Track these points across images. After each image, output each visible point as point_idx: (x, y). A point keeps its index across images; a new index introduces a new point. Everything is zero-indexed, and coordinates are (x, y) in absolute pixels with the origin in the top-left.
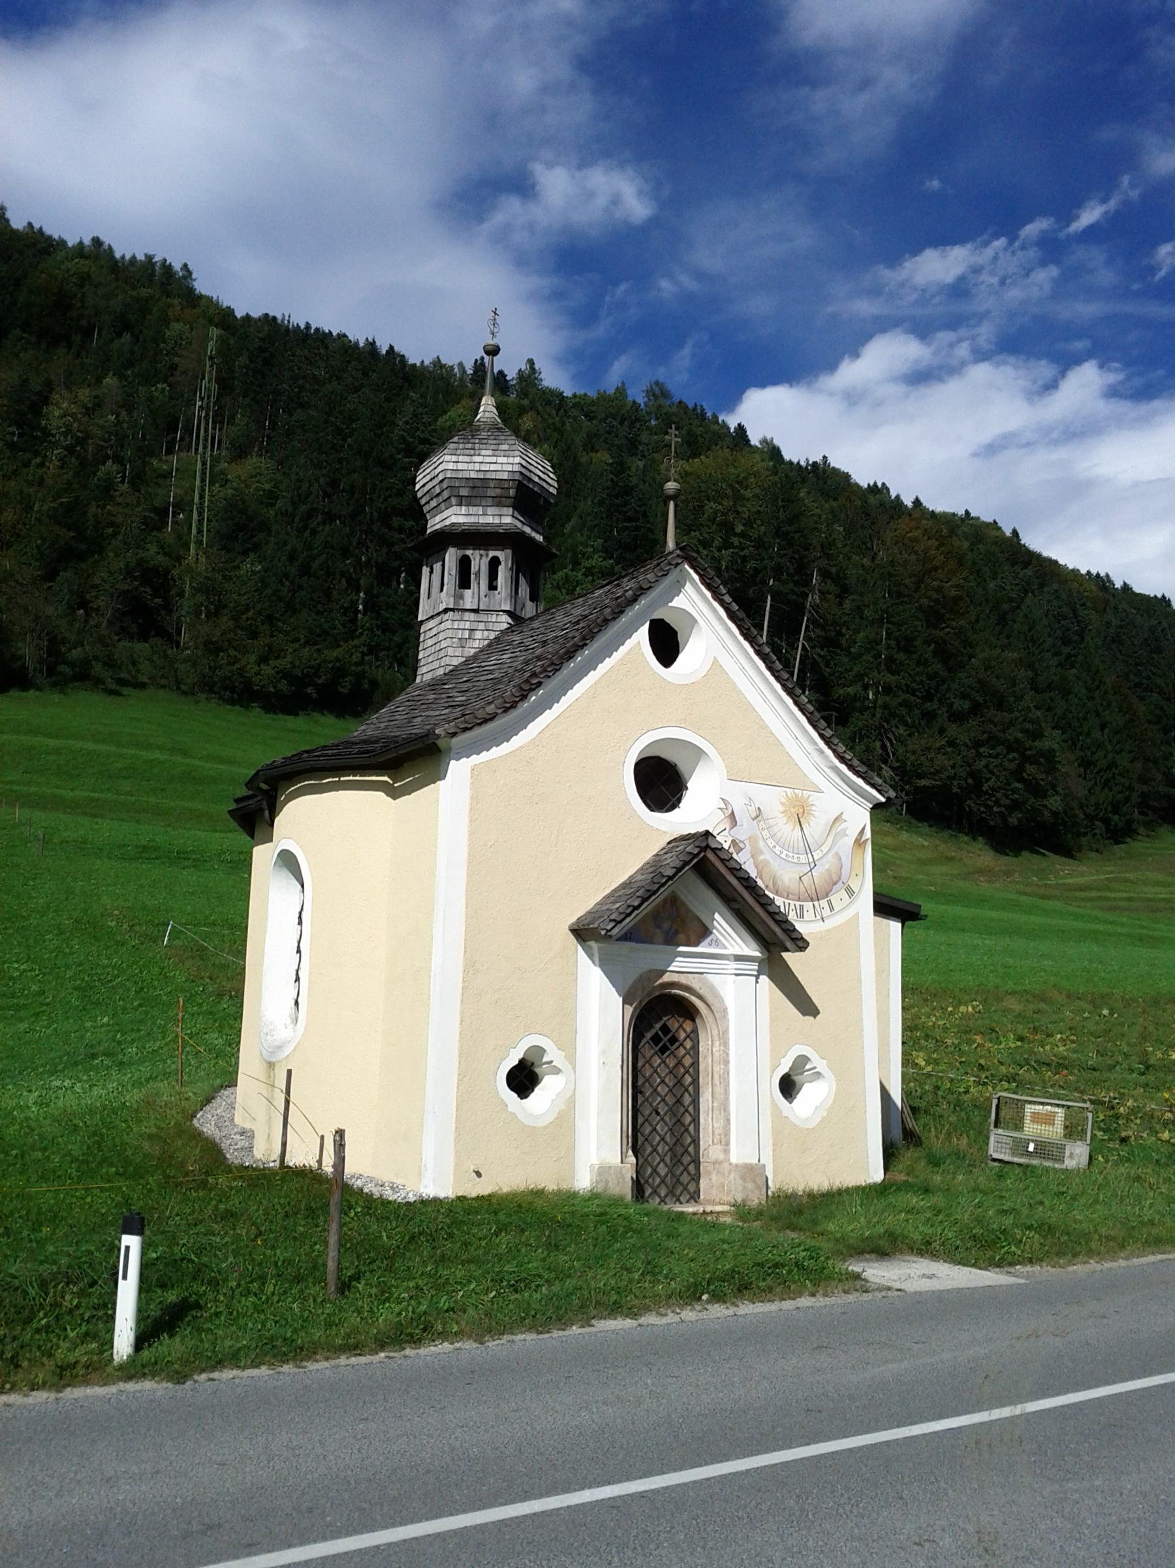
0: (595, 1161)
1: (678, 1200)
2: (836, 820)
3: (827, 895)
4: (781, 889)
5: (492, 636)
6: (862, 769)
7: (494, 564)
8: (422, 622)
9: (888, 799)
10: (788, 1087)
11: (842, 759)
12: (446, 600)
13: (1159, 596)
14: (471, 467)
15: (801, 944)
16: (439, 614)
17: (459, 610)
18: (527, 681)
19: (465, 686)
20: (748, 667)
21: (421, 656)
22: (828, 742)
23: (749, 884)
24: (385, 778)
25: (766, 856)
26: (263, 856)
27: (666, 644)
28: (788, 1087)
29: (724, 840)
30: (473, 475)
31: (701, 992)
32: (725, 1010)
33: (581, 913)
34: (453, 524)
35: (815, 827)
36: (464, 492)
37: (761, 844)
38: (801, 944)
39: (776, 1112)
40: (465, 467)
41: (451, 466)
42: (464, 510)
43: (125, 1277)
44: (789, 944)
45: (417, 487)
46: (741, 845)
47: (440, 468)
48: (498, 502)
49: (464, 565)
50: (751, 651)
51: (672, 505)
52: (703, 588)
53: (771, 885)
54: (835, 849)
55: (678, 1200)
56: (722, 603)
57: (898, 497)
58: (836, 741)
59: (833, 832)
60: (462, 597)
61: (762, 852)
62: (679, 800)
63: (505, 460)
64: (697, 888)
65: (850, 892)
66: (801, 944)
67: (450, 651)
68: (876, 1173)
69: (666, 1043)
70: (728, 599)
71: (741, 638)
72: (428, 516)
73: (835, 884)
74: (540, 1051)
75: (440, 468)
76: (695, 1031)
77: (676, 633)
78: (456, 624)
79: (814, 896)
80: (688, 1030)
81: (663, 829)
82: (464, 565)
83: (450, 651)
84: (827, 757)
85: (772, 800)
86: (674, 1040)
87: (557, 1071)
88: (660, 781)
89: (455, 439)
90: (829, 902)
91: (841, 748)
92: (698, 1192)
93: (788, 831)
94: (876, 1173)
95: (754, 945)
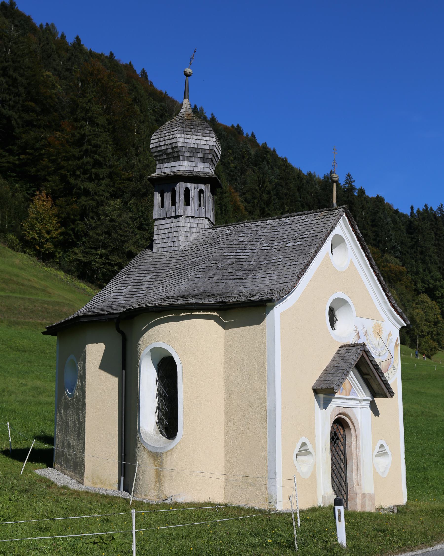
0: (323, 493)
6: (400, 311)
8: (155, 219)
9: (407, 325)
14: (191, 141)
30: (192, 146)
36: (187, 154)
38: (392, 394)
40: (188, 141)
41: (181, 140)
43: (340, 520)
48: (204, 159)
49: (187, 191)
60: (187, 210)
63: (208, 139)
65: (394, 368)
68: (400, 497)
71: (361, 249)
73: (390, 365)
82: (187, 191)
84: (387, 305)
85: (369, 325)
94: (400, 497)
95: (369, 394)
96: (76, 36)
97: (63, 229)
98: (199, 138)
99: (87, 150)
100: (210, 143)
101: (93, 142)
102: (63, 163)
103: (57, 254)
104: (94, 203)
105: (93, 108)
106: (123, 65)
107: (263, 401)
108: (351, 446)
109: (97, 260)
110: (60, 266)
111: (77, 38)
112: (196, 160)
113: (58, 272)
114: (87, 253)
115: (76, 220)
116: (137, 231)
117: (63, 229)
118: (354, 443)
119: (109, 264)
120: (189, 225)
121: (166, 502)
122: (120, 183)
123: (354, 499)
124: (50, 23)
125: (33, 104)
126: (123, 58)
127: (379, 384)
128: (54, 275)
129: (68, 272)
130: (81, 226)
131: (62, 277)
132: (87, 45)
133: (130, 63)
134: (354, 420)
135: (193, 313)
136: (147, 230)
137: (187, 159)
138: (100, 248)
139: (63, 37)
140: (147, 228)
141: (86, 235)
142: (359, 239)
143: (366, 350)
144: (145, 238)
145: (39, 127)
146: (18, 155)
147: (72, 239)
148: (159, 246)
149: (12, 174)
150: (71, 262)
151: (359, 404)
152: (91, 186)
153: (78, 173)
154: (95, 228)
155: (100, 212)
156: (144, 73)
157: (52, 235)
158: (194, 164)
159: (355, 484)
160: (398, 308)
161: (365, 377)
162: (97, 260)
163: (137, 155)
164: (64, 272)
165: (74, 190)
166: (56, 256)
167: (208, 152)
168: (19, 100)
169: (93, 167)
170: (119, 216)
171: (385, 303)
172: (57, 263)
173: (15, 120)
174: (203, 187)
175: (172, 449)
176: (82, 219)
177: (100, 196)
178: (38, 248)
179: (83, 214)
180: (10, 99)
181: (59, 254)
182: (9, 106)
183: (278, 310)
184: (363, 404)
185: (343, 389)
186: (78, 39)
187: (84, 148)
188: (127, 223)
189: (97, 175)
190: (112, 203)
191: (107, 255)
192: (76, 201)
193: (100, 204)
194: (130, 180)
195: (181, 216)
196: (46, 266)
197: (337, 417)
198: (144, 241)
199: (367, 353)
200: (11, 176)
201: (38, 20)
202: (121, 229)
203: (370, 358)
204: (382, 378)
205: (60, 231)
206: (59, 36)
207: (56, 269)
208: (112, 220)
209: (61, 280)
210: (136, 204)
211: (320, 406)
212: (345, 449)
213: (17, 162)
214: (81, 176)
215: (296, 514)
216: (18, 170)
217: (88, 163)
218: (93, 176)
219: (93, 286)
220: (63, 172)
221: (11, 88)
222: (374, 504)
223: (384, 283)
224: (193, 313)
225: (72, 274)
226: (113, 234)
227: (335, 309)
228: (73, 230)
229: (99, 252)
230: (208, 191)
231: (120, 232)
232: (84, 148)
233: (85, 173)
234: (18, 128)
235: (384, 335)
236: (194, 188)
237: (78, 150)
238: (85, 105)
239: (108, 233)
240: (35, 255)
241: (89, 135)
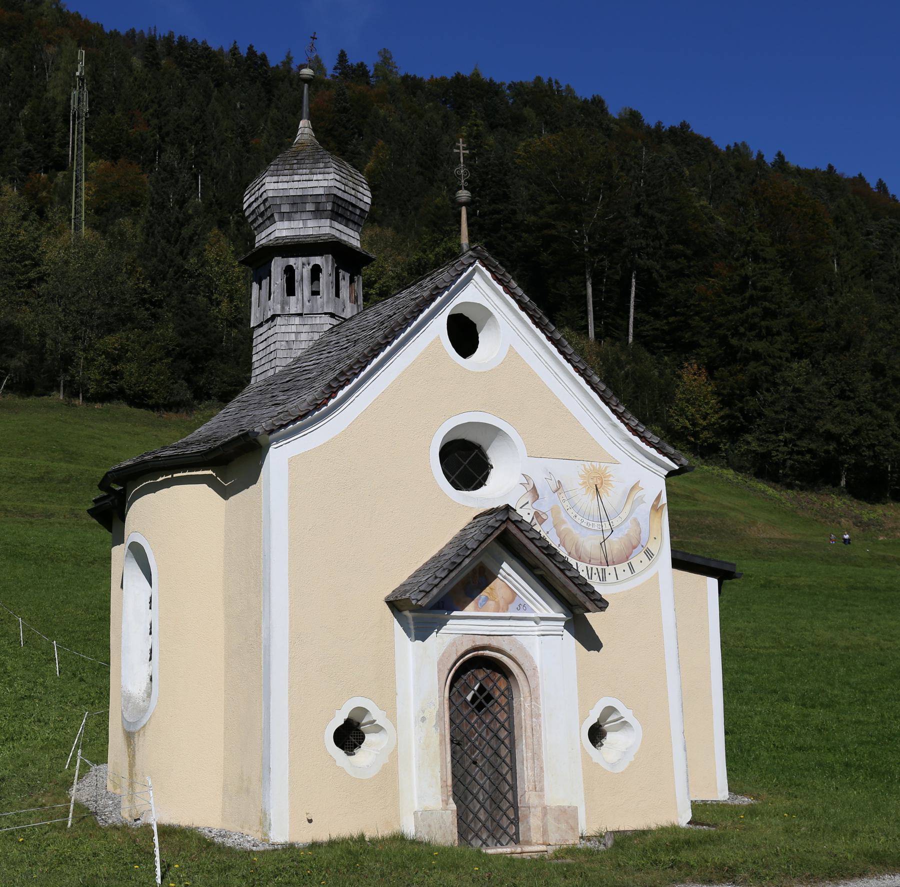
0: (416, 807)
1: (499, 842)
2: (633, 488)
3: (627, 558)
4: (583, 555)
5: (316, 337)
6: (656, 440)
7: (316, 271)
10: (596, 734)
11: (635, 432)
14: (290, 185)
16: (267, 321)
18: (336, 379)
19: (286, 386)
20: (542, 352)
21: (255, 358)
22: (620, 416)
23: (551, 552)
24: (210, 472)
25: (568, 525)
26: (119, 553)
27: (464, 335)
28: (596, 734)
29: (526, 514)
30: (292, 193)
31: (511, 653)
32: (535, 669)
33: (396, 585)
34: (277, 238)
35: (612, 497)
36: (285, 208)
37: (563, 515)
39: (586, 759)
40: (285, 186)
41: (273, 186)
44: (589, 605)
45: (245, 206)
46: (544, 517)
48: (318, 213)
49: (289, 271)
50: (543, 337)
51: (464, 210)
52: (495, 283)
53: (573, 552)
54: (633, 516)
55: (499, 842)
56: (513, 295)
58: (629, 416)
59: (630, 501)
60: (288, 304)
61: (564, 522)
62: (485, 478)
63: (320, 177)
65: (649, 554)
66: (601, 604)
69: (483, 700)
70: (520, 292)
71: (533, 327)
72: (256, 233)
73: (634, 548)
74: (364, 711)
76: (509, 689)
77: (475, 325)
78: (288, 327)
79: (604, 561)
80: (503, 687)
81: (470, 505)
82: (289, 271)
85: (571, 473)
86: (489, 698)
87: (379, 729)
88: (465, 461)
89: (276, 161)
91: (634, 422)
92: (517, 833)
93: (588, 501)
95: (558, 607)
96: (776, 152)
97: (726, 411)
98: (304, 177)
99: (751, 296)
100: (325, 184)
101: (759, 285)
102: (722, 320)
103: (721, 446)
104: (767, 369)
105: (755, 238)
106: (848, 180)
109: (780, 449)
110: (727, 463)
112: (304, 216)
113: (725, 471)
114: (764, 440)
115: (744, 396)
116: (837, 401)
117: (726, 411)
119: (799, 453)
120: (294, 329)
121: (138, 822)
122: (805, 337)
124: (739, 142)
125: (681, 247)
126: (847, 170)
128: (718, 475)
129: (739, 469)
130: (752, 403)
131: (730, 477)
132: (794, 160)
133: (860, 175)
134: (520, 661)
135: (175, 475)
136: (853, 398)
137: (284, 216)
138: (782, 431)
139: (760, 156)
140: (852, 395)
141: (761, 415)
142: (523, 307)
144: (849, 411)
145: (689, 276)
146: (666, 317)
147: (741, 423)
149: (660, 344)
150: (742, 454)
151: (536, 628)
152: (760, 346)
153: (742, 330)
154: (773, 403)
155: (777, 381)
156: (881, 185)
157: (710, 420)
158: (300, 224)
160: (649, 435)
162: (780, 449)
163: (831, 294)
164: (734, 470)
165: (739, 355)
166: (720, 449)
167: (324, 199)
168: (661, 245)
169: (763, 319)
170: (807, 382)
171: (615, 426)
172: (723, 458)
173: (657, 271)
174: (317, 260)
175: (145, 726)
176: (753, 394)
177: (774, 357)
178: (693, 439)
179: (754, 386)
180: (648, 245)
181: (725, 445)
182: (647, 254)
184: (542, 628)
185: (487, 599)
186: (780, 156)
187: (747, 295)
188: (820, 392)
189: (768, 329)
190: (795, 365)
191: (794, 440)
192: (742, 369)
193: (775, 369)
194: (822, 330)
195: (279, 315)
196: (707, 463)
198: (850, 415)
199: (519, 525)
200: (659, 348)
201: (722, 143)
202: (810, 402)
203: (527, 534)
204: (567, 573)
205: (722, 413)
206: (754, 157)
207: (722, 467)
208: (796, 390)
209: (728, 481)
210: (832, 364)
211: (409, 635)
212: (510, 718)
213: (666, 328)
214: (748, 333)
216: (668, 338)
217: (754, 314)
218: (764, 331)
219: (778, 486)
220: (721, 332)
221: (647, 230)
222: (574, 828)
224: (175, 475)
225: (746, 472)
226: (798, 409)
227: (484, 446)
228: (741, 410)
229: (781, 437)
230: (328, 266)
231: (810, 405)
232: (747, 295)
233: (752, 327)
234: (663, 281)
236: (302, 266)
237: (740, 298)
238: (743, 236)
239: (792, 409)
240: (690, 450)
241: (753, 276)
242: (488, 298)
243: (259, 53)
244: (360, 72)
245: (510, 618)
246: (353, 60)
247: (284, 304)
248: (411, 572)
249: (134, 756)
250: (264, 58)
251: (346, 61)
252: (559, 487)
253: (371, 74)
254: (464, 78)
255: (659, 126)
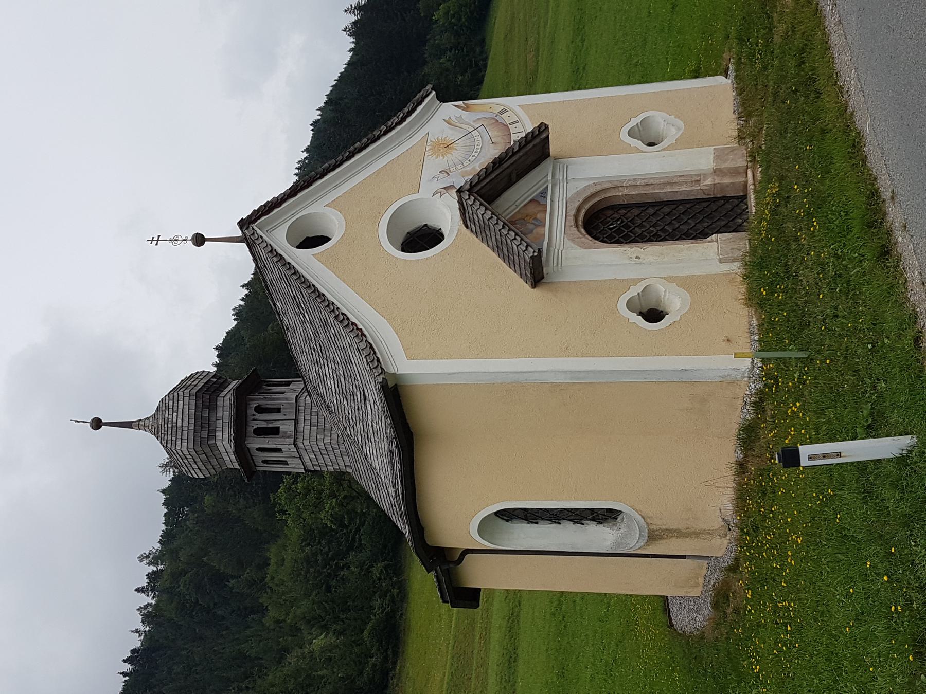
1: (744, 210)
6: (410, 106)
7: (260, 410)
9: (433, 89)
11: (403, 119)
12: (286, 445)
13: (312, 128)
15: (543, 128)
17: (296, 435)
23: (497, 163)
28: (654, 315)
36: (205, 434)
42: (219, 434)
43: (839, 455)
44: (544, 135)
47: (186, 453)
57: (243, 299)
60: (285, 433)
64: (501, 184)
65: (503, 112)
67: (327, 440)
75: (186, 453)
77: (307, 238)
82: (260, 432)
83: (327, 440)
85: (433, 164)
90: (511, 124)
93: (455, 155)
107: (556, 387)
108: (632, 196)
111: (243, 286)
118: (626, 192)
120: (307, 428)
123: (723, 187)
127: (526, 153)
143: (468, 186)
148: (341, 464)
159: (696, 188)
160: (406, 110)
161: (514, 176)
183: (402, 364)
197: (583, 230)
212: (638, 205)
215: (764, 361)
222: (733, 150)
223: (365, 140)
235: (450, 134)
242: (285, 221)
243: (129, 654)
244: (152, 576)
245: (552, 201)
246: (144, 582)
247: (286, 436)
248: (510, 271)
249: (671, 531)
250: (133, 651)
251: (143, 587)
252: (446, 172)
253: (155, 569)
254: (166, 500)
255: (216, 365)
